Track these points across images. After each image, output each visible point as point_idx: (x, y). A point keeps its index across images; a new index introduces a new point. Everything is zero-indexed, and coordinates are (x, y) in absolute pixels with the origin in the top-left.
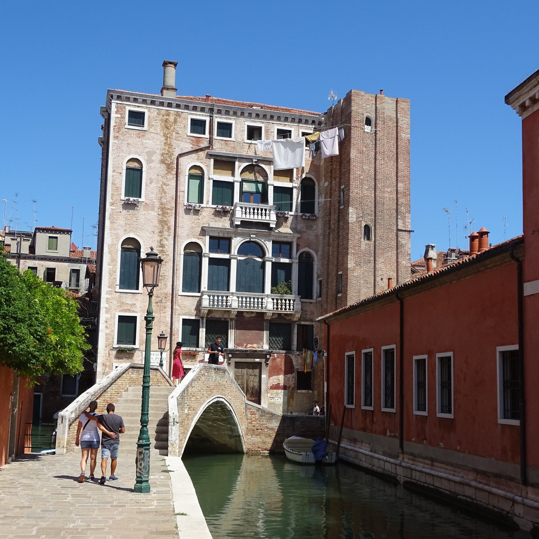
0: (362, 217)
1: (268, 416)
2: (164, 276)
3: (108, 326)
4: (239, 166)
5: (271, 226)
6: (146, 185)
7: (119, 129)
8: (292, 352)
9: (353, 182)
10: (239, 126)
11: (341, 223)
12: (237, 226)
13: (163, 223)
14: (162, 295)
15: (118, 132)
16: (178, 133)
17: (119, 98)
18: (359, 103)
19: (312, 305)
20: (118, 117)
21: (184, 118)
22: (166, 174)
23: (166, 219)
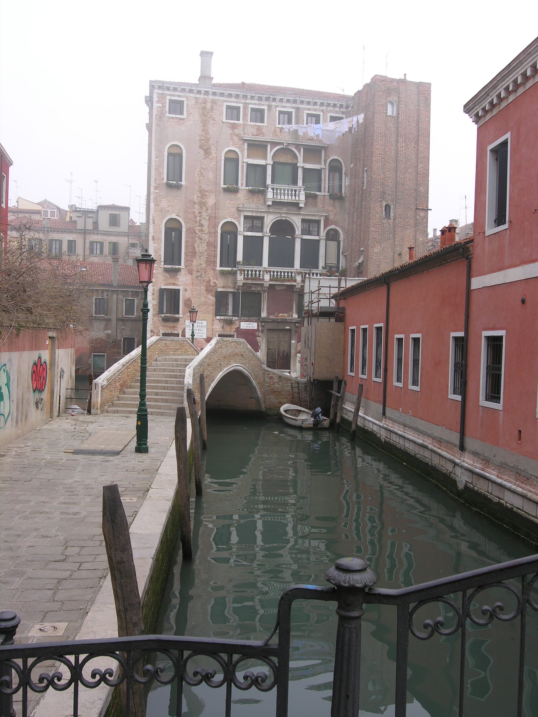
11: (364, 203)
12: (269, 206)
16: (214, 120)
17: (160, 88)
20: (159, 107)
22: (204, 158)
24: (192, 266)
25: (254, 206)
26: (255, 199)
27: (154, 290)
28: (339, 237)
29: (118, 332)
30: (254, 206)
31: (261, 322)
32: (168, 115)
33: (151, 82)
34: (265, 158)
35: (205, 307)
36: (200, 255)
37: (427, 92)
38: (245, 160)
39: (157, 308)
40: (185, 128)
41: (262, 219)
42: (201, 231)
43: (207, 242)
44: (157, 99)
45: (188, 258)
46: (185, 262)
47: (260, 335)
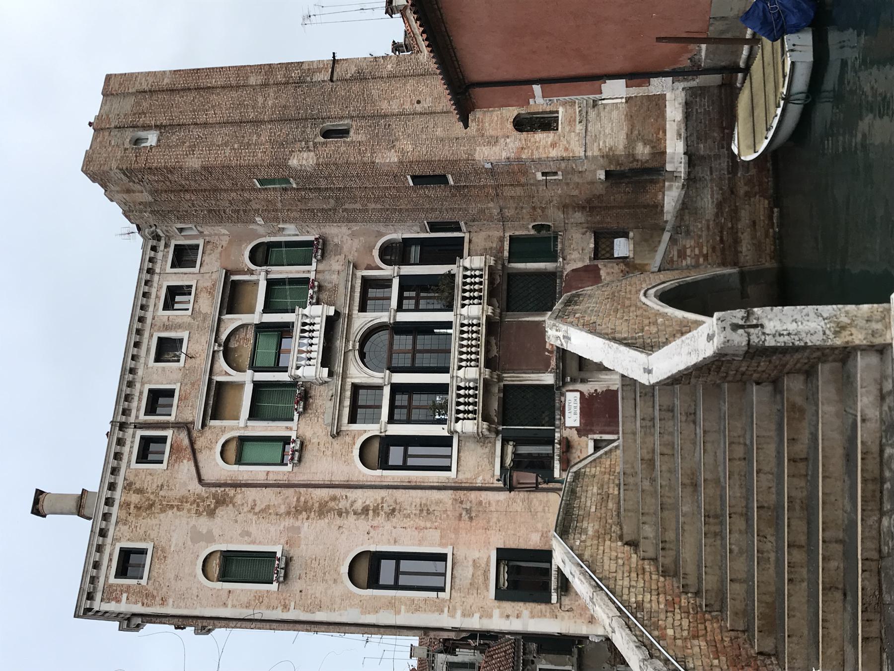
0: (306, 143)
1: (687, 217)
2: (421, 505)
3: (516, 612)
4: (227, 374)
5: (332, 313)
6: (253, 542)
7: (147, 596)
9: (245, 160)
10: (155, 377)
11: (323, 184)
12: (331, 374)
13: (323, 510)
14: (457, 509)
15: (154, 597)
16: (162, 485)
17: (90, 597)
18: (106, 158)
19: (473, 239)
20: (128, 599)
21: (136, 475)
22: (234, 505)
23: (317, 505)
28: (396, 244)
31: (565, 384)
32: (144, 582)
33: (76, 615)
34: (240, 386)
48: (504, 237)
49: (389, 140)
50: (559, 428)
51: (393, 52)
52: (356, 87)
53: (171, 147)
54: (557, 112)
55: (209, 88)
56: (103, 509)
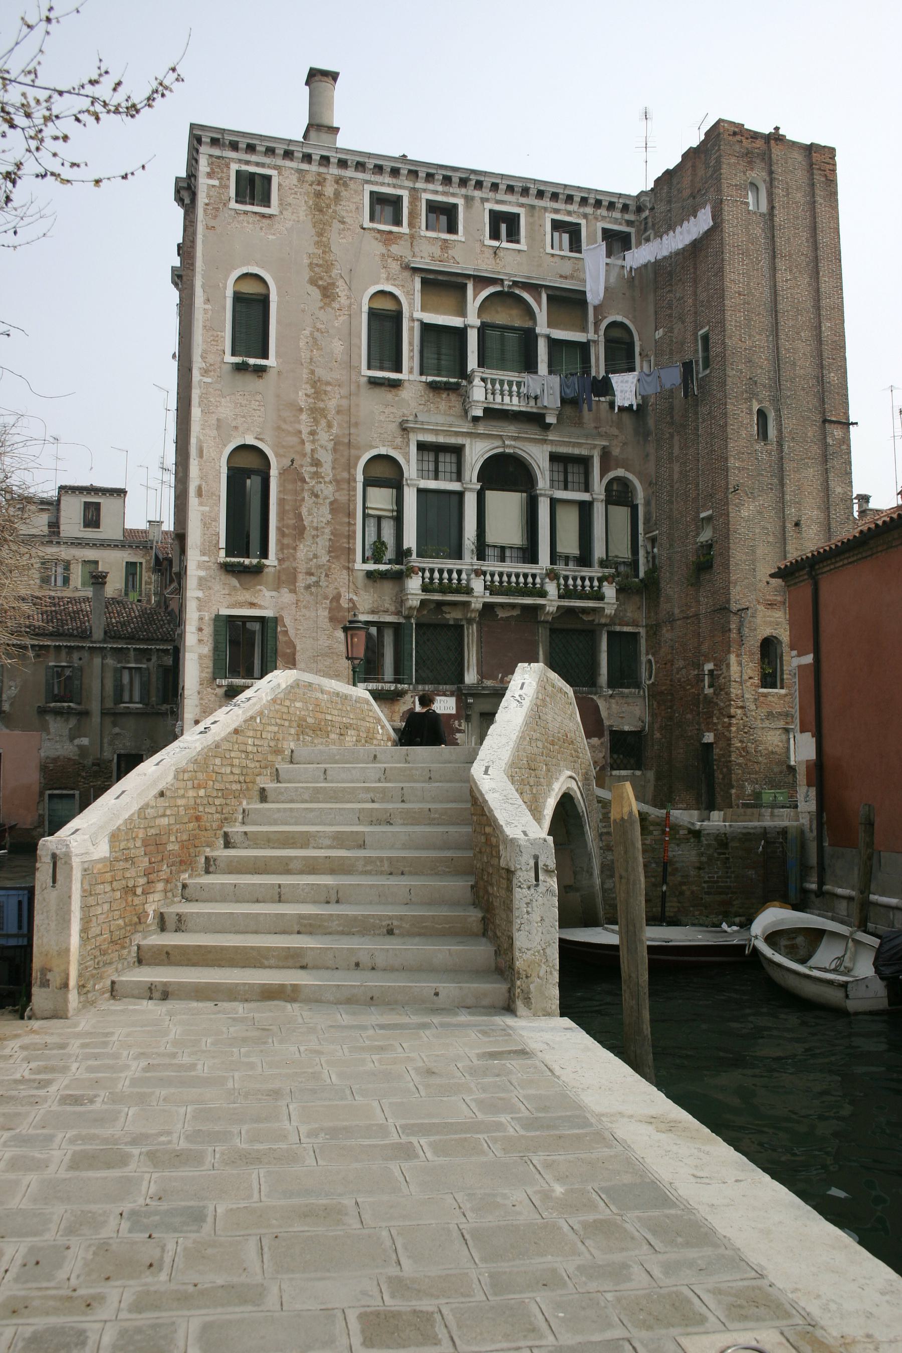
7: (215, 209)
8: (599, 690)
9: (731, 316)
12: (476, 419)
14: (320, 571)
16: (343, 223)
17: (215, 142)
20: (213, 186)
22: (321, 308)
24: (295, 559)
25: (440, 419)
26: (443, 405)
27: (201, 619)
28: (632, 497)
29: (106, 740)
30: (440, 419)
32: (233, 205)
33: (193, 126)
34: (462, 312)
35: (329, 661)
36: (314, 533)
37: (828, 167)
38: (418, 315)
39: (210, 663)
40: (274, 237)
41: (457, 451)
42: (316, 475)
43: (331, 503)
44: (208, 170)
45: (286, 541)
46: (277, 551)
47: (463, 728)
48: (637, 626)
49: (753, 489)
50: (415, 689)
51: (858, 495)
52: (816, 450)
53: (747, 228)
54: (782, 688)
55: (818, 273)
56: (316, 154)
